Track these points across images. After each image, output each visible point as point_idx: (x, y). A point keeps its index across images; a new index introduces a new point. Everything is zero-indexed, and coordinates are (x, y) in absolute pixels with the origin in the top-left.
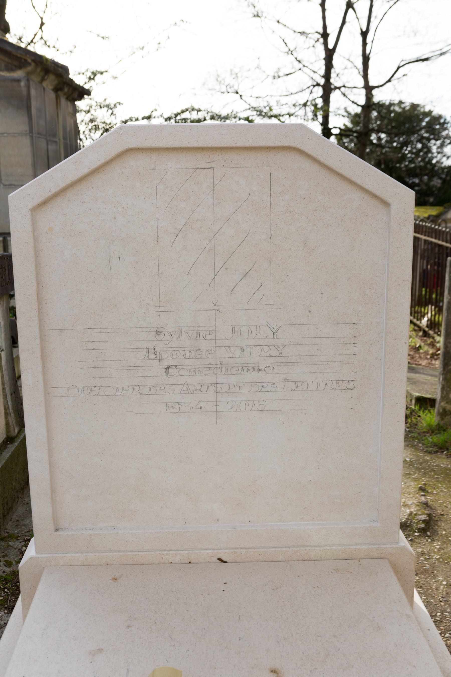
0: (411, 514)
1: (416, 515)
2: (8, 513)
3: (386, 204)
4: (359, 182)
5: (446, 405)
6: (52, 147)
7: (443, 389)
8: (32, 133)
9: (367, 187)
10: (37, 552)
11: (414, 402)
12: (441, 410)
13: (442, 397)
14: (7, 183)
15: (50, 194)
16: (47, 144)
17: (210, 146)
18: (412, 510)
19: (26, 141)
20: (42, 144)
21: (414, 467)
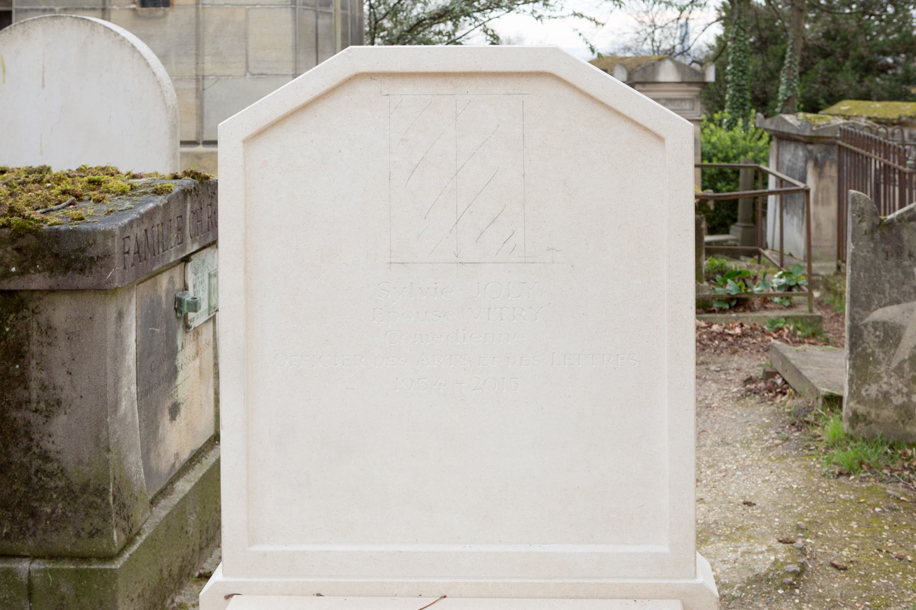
0: (776, 560)
1: (782, 564)
2: (207, 546)
3: (660, 139)
4: (626, 112)
5: (858, 406)
6: (323, 22)
7: (851, 381)
8: (295, 4)
9: (635, 119)
10: (224, 575)
11: (820, 401)
12: (851, 414)
13: (850, 393)
14: (256, 72)
15: (265, 123)
16: (317, 17)
17: (451, 70)
18: (779, 556)
20: (310, 17)
21: (800, 496)
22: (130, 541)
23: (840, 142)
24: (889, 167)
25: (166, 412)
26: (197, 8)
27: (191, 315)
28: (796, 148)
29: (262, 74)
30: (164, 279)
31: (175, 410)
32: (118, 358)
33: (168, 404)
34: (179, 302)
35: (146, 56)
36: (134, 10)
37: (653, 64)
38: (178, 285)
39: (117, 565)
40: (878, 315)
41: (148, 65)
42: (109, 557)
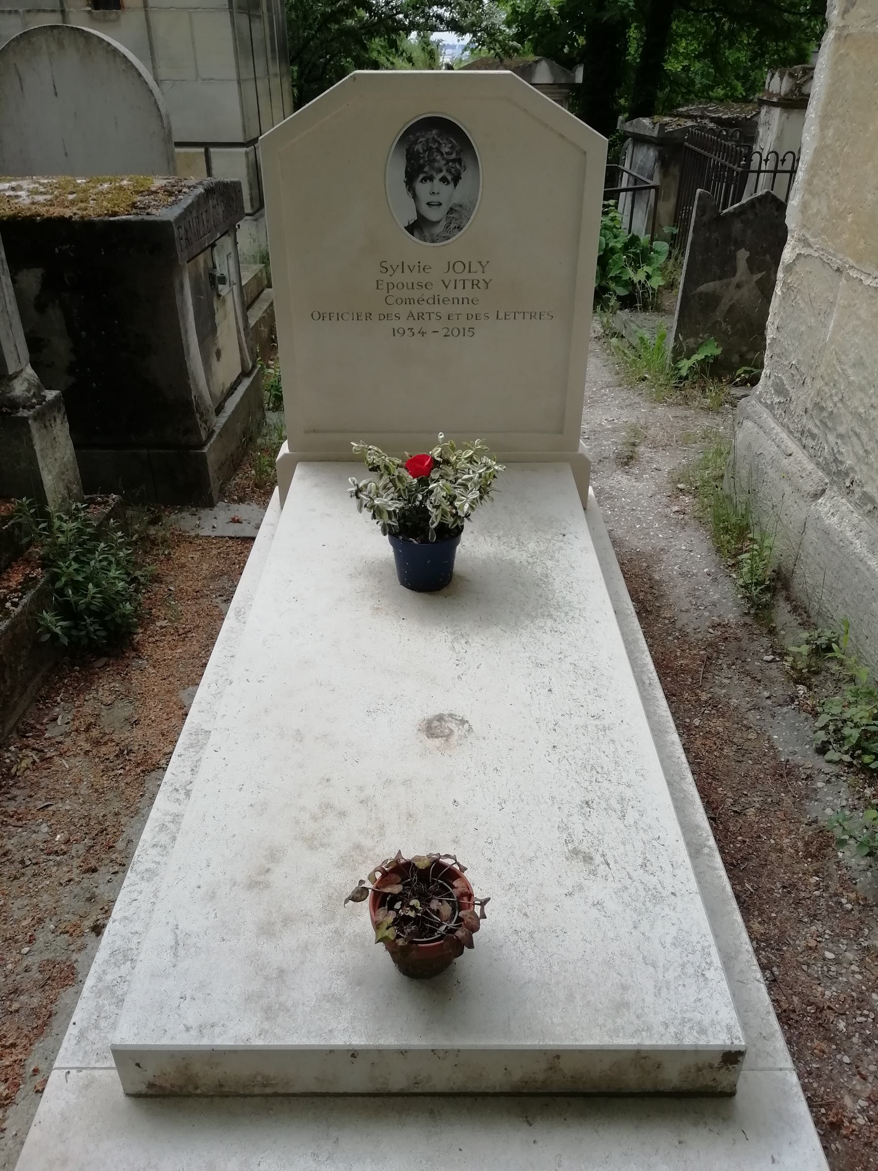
6: (257, 25)
19: (226, 18)
22: (209, 437)
23: (686, 144)
24: (726, 166)
25: (214, 355)
26: (146, 11)
27: (220, 287)
28: (649, 149)
29: (211, 79)
30: (201, 258)
31: (218, 354)
32: (185, 317)
33: (215, 350)
34: (212, 277)
35: (137, 67)
36: (89, 12)
37: (530, 66)
38: (210, 265)
39: (205, 450)
40: (703, 288)
41: (140, 75)
42: (202, 445)
